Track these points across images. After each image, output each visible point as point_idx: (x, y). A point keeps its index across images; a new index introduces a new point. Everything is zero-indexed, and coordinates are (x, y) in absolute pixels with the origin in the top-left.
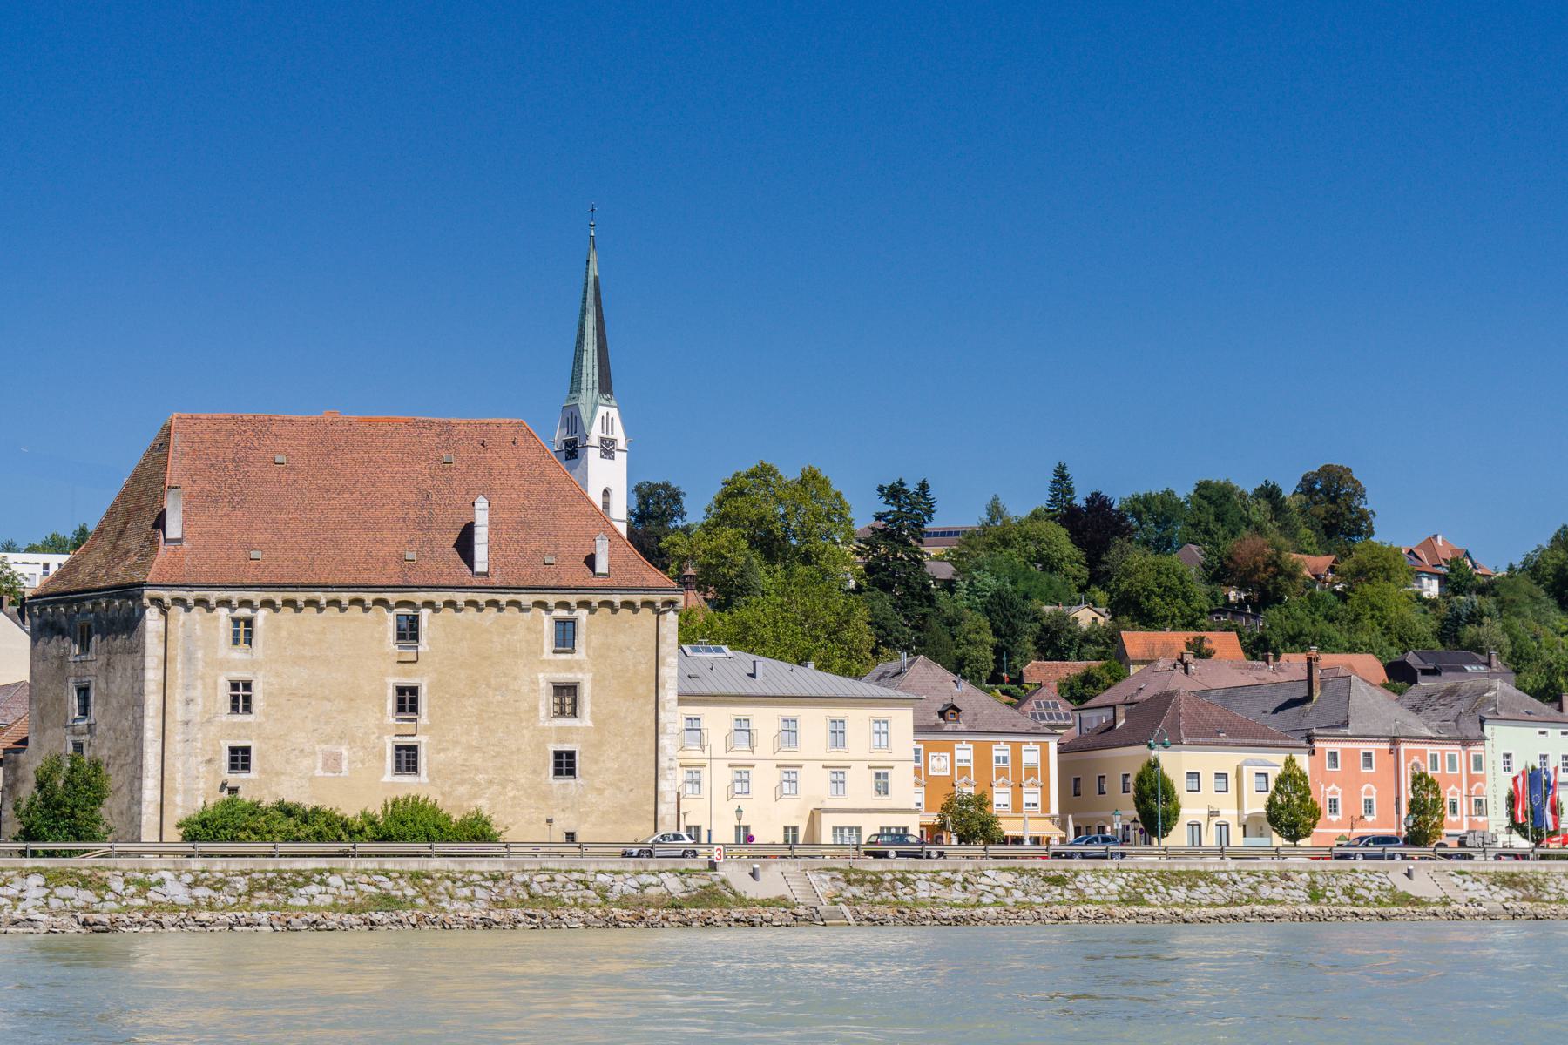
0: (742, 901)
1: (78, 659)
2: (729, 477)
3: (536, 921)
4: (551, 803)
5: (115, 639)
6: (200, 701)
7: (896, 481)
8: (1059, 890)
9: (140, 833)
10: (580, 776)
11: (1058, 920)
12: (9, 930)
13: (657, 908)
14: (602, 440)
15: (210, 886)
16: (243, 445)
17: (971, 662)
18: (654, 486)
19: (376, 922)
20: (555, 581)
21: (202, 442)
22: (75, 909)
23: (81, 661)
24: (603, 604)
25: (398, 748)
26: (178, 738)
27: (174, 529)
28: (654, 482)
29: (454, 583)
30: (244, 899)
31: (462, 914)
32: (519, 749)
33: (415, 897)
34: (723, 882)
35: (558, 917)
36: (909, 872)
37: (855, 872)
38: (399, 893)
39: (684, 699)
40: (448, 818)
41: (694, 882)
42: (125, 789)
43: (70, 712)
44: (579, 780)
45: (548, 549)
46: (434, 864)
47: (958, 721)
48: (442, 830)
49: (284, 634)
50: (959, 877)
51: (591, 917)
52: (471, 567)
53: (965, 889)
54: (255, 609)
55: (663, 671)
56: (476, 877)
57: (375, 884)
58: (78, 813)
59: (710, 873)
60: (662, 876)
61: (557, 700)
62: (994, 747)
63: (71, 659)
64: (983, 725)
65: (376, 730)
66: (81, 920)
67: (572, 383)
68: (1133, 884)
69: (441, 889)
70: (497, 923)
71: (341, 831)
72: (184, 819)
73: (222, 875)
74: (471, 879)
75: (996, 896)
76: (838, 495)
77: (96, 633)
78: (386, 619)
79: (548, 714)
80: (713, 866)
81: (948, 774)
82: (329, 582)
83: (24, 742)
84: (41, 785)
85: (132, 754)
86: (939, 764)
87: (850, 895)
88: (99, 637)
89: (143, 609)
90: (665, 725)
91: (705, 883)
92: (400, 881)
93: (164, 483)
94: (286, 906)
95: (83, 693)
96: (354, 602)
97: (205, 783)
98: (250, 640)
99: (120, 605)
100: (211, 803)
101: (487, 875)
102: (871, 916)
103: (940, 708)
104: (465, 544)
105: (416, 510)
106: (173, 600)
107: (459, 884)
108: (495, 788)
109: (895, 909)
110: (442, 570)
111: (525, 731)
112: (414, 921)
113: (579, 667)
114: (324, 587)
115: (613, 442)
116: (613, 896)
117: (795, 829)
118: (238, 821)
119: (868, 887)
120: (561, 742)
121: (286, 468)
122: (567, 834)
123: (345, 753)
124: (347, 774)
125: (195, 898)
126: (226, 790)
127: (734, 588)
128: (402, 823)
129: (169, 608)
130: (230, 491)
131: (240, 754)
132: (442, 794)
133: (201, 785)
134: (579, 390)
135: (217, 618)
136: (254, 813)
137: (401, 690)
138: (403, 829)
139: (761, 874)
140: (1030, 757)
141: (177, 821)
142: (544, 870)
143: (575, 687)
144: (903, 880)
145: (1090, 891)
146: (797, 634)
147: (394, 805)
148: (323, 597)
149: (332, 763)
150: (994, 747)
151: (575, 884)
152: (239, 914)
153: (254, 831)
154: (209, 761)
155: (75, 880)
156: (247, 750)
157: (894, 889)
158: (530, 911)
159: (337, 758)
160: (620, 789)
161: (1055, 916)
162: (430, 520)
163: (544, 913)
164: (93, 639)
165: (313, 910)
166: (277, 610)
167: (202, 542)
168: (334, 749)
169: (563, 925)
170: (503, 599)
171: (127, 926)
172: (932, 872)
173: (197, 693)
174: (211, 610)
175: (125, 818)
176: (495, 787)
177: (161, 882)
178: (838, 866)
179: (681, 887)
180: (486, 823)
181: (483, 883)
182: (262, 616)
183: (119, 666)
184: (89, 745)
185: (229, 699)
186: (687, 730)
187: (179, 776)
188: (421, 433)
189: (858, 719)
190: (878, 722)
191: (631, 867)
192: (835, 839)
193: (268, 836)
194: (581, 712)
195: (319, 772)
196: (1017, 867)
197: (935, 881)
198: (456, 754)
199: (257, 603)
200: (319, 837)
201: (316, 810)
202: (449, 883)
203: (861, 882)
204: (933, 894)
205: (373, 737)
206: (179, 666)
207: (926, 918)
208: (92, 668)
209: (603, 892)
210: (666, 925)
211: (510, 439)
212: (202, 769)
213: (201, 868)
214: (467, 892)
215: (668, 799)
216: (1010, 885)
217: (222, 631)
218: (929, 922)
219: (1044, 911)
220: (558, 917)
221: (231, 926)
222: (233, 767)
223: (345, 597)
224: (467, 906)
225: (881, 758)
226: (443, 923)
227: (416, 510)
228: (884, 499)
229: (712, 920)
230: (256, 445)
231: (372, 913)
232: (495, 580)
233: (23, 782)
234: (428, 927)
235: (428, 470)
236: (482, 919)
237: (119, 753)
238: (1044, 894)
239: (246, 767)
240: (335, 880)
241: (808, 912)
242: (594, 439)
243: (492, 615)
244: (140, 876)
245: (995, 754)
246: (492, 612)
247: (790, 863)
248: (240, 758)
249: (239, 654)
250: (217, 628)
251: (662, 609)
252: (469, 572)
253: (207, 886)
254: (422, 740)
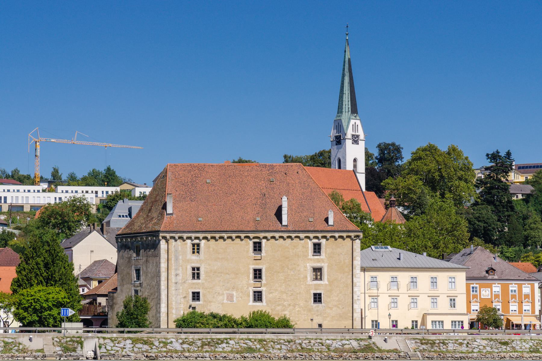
0: (380, 351)
1: (135, 259)
2: (415, 151)
3: (303, 357)
4: (313, 313)
5: (149, 251)
6: (181, 275)
7: (495, 151)
8: (505, 347)
9: (160, 324)
10: (324, 303)
11: (501, 358)
12: (122, 358)
13: (347, 353)
14: (353, 135)
15: (188, 344)
16: (194, 176)
17: (532, 238)
18: (387, 144)
19: (246, 357)
20: (313, 228)
21: (179, 175)
22: (143, 352)
23: (137, 260)
24: (331, 237)
25: (255, 292)
26: (173, 289)
27: (170, 210)
28: (387, 142)
29: (274, 229)
30: (200, 348)
31: (277, 354)
32: (300, 293)
33: (260, 348)
34: (374, 343)
35: (311, 356)
36: (446, 340)
37: (425, 340)
38: (255, 347)
39: (364, 270)
40: (273, 319)
41: (362, 343)
42: (154, 308)
43: (133, 278)
44: (323, 304)
45: (311, 216)
46: (267, 336)
47: (494, 275)
48: (271, 324)
49: (211, 249)
50: (466, 342)
51: (323, 356)
52: (281, 223)
53: (467, 346)
54: (200, 240)
55: (355, 263)
56: (282, 341)
57: (246, 344)
58: (139, 317)
59: (369, 340)
60: (351, 341)
61: (314, 273)
62: (510, 286)
63: (133, 259)
64: (505, 276)
65: (246, 285)
66: (146, 355)
67: (338, 109)
68: (536, 345)
69: (269, 345)
70: (289, 358)
71: (233, 324)
72: (176, 319)
73: (192, 340)
74: (280, 342)
75: (480, 349)
76: (466, 158)
77: (142, 249)
78: (249, 244)
79: (311, 279)
80: (370, 337)
81: (490, 297)
82: (228, 230)
83: (116, 289)
84: (125, 307)
85: (156, 294)
86: (485, 293)
87: (422, 349)
88: (143, 250)
89: (159, 241)
90: (356, 283)
91: (367, 344)
92: (255, 342)
93: (165, 191)
94: (215, 351)
95: (137, 271)
96: (237, 237)
97: (184, 305)
98: (199, 252)
99: (151, 239)
100: (186, 313)
101: (286, 340)
102: (428, 356)
103: (487, 269)
104: (279, 214)
105: (260, 200)
106: (170, 237)
107: (276, 343)
108: (291, 307)
109: (438, 354)
110: (270, 224)
111: (302, 286)
112: (259, 356)
113: (322, 260)
114: (226, 232)
115: (358, 136)
116: (332, 348)
117: (416, 322)
118: (196, 320)
119: (429, 345)
120: (316, 290)
121: (211, 185)
122: (319, 325)
123: (235, 294)
124: (236, 302)
125: (183, 348)
126: (191, 308)
127: (416, 204)
128: (256, 321)
129: (169, 240)
130: (190, 194)
131: (196, 295)
132: (271, 309)
133: (182, 306)
134: (342, 112)
135: (186, 244)
136: (202, 317)
137: (255, 270)
138: (257, 323)
139: (388, 340)
140: (526, 290)
141: (174, 320)
142: (307, 339)
143: (321, 269)
144: (443, 343)
145: (517, 347)
146: (433, 233)
147: (253, 314)
148: (225, 235)
149: (230, 298)
150: (510, 286)
151: (318, 344)
152: (199, 354)
153: (202, 324)
154: (185, 297)
155: (142, 342)
156: (198, 293)
157: (439, 346)
158: (301, 354)
159: (232, 296)
160: (339, 308)
161: (500, 357)
162: (265, 204)
163: (306, 354)
164: (141, 251)
165: (224, 353)
166: (208, 240)
167: (180, 214)
168: (231, 293)
169: (313, 359)
170: (293, 235)
171: (161, 358)
172: (455, 340)
173: (180, 272)
174: (184, 241)
175: (154, 319)
176: (291, 307)
177: (171, 342)
178: (418, 338)
179: (358, 345)
180: (288, 321)
181: (284, 343)
182: (203, 243)
183: (151, 262)
184: (140, 291)
185: (191, 274)
186: (371, 282)
187: (174, 303)
188: (262, 170)
189: (443, 277)
190: (451, 278)
191: (339, 338)
192: (433, 327)
193: (207, 326)
194: (324, 278)
195: (225, 301)
196: (490, 338)
197: (456, 343)
198: (276, 294)
199: (201, 238)
200: (226, 326)
201: (224, 316)
202: (272, 343)
203: (426, 344)
204: (455, 348)
205: (245, 288)
206: (173, 262)
207: (449, 357)
208: (141, 262)
209: (328, 347)
210: (350, 359)
211: (296, 171)
212: (182, 300)
213: (185, 338)
214: (279, 346)
215: (357, 311)
216: (485, 345)
217: (188, 248)
218: (450, 359)
219: (496, 355)
220: (311, 356)
221: (196, 358)
222: (194, 299)
223: (234, 235)
224: (279, 351)
225: (452, 293)
226: (270, 357)
227: (260, 200)
228: (489, 160)
229: (367, 357)
230: (199, 175)
231: (245, 354)
232: (290, 228)
233: (116, 304)
234: (264, 359)
235: (264, 185)
236: (283, 356)
237: (152, 294)
238: (499, 348)
239: (198, 299)
240: (232, 342)
241: (404, 355)
242: (349, 135)
243: (289, 242)
244: (164, 340)
245: (511, 289)
246: (289, 240)
247: (399, 336)
248: (196, 296)
249: (195, 257)
250: (186, 247)
251: (354, 239)
252: (280, 225)
253: (187, 344)
254: (263, 289)
